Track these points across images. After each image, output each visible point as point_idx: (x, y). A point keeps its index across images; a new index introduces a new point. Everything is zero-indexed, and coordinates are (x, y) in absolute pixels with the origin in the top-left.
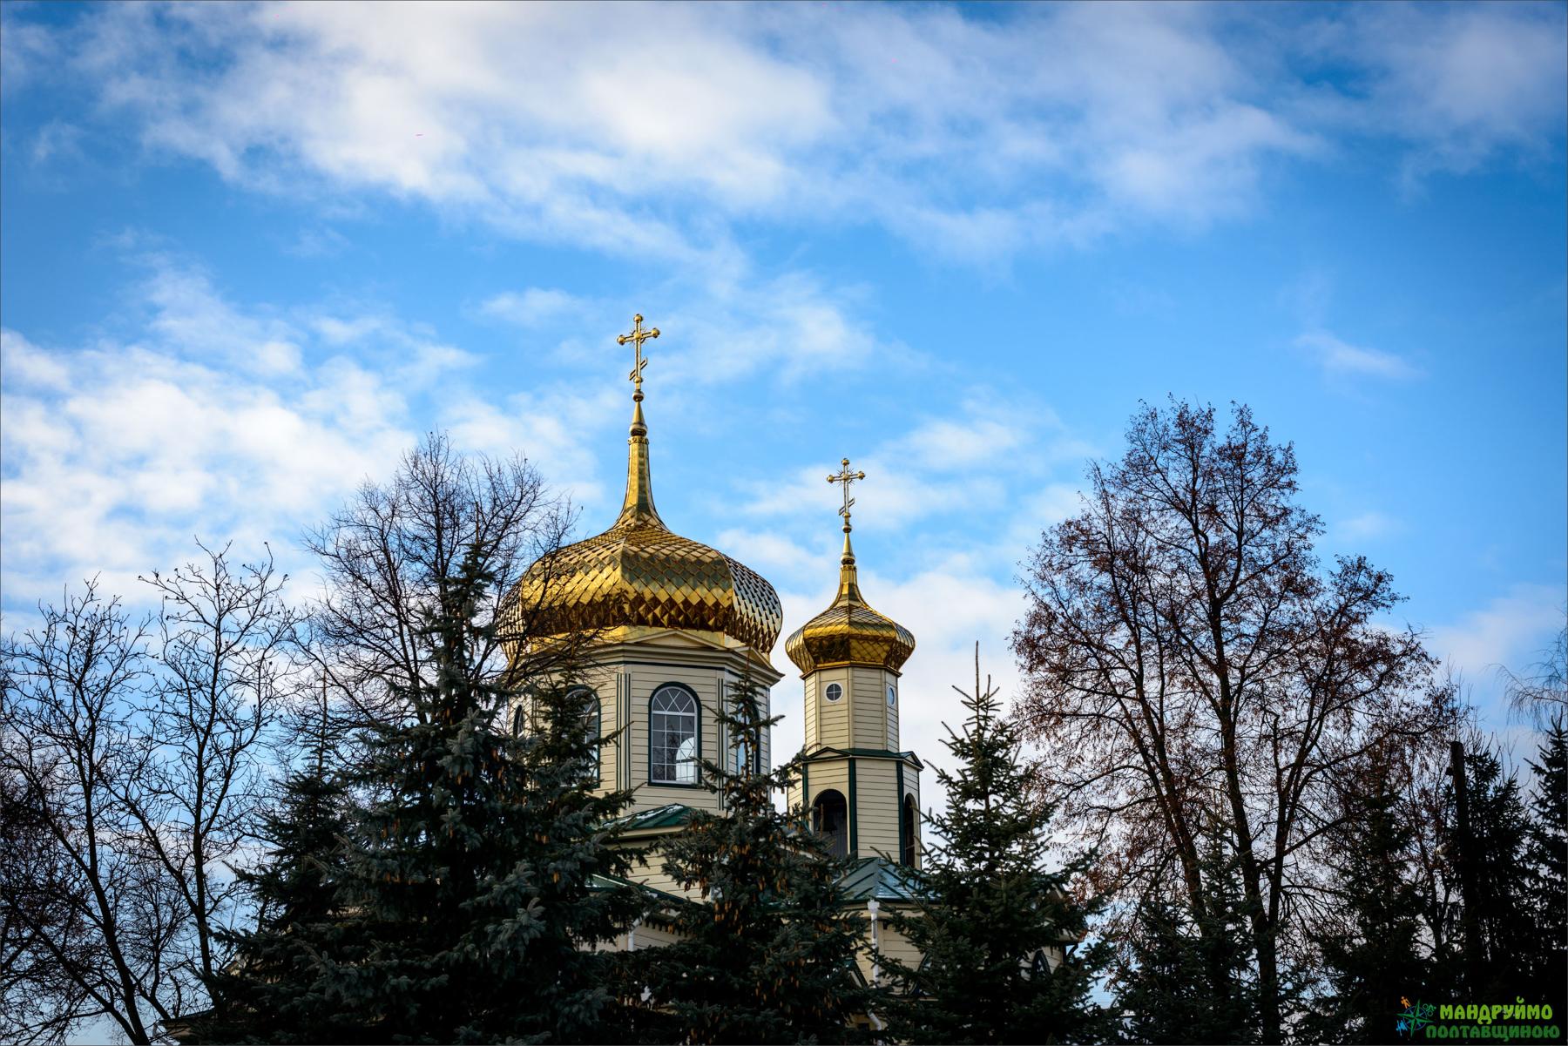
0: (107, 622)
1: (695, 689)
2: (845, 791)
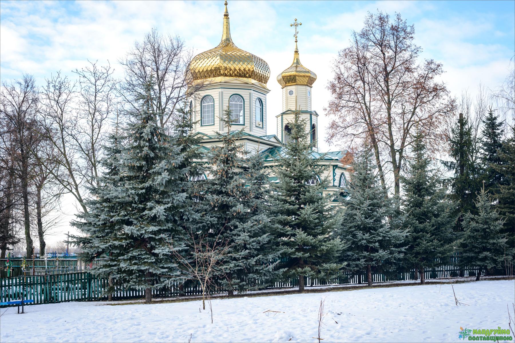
0: (64, 84)
1: (242, 96)
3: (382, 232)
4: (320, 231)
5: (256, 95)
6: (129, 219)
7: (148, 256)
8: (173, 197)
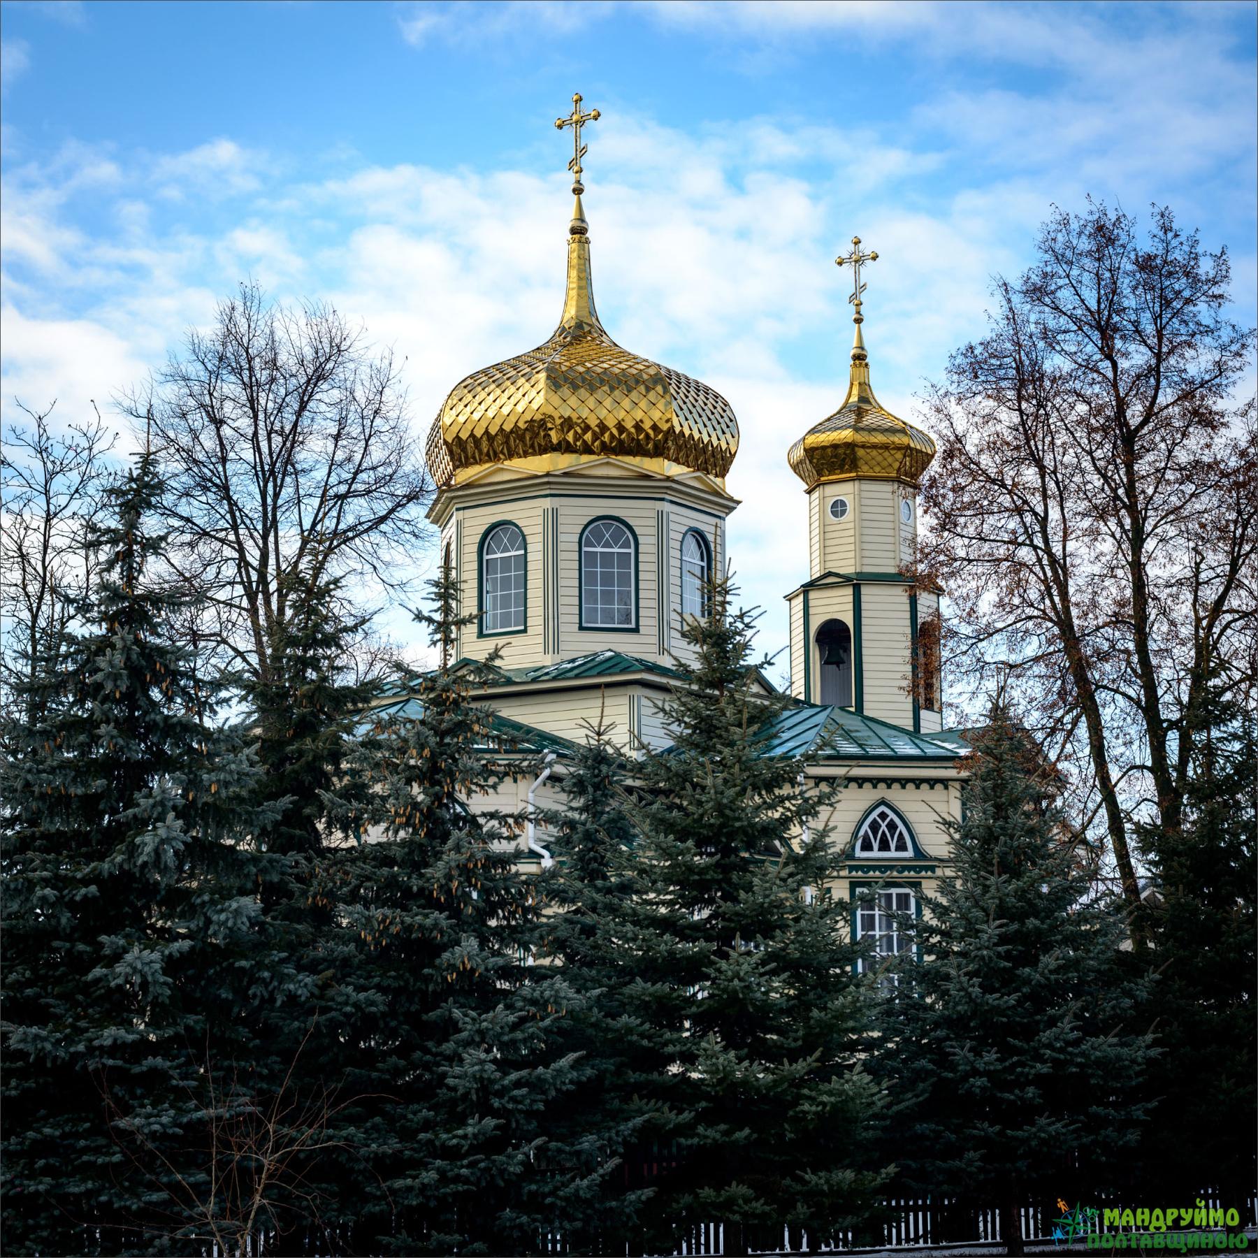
1: (631, 522)
2: (849, 620)
3: (1050, 1046)
4: (795, 1040)
5: (681, 519)
6: (39, 996)
7: (102, 1141)
8: (205, 914)
